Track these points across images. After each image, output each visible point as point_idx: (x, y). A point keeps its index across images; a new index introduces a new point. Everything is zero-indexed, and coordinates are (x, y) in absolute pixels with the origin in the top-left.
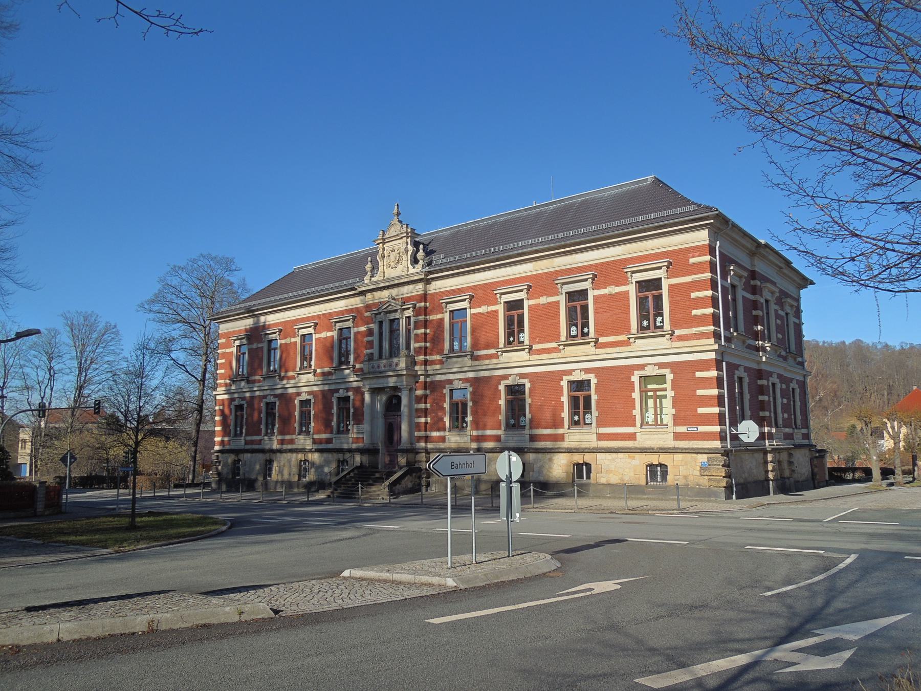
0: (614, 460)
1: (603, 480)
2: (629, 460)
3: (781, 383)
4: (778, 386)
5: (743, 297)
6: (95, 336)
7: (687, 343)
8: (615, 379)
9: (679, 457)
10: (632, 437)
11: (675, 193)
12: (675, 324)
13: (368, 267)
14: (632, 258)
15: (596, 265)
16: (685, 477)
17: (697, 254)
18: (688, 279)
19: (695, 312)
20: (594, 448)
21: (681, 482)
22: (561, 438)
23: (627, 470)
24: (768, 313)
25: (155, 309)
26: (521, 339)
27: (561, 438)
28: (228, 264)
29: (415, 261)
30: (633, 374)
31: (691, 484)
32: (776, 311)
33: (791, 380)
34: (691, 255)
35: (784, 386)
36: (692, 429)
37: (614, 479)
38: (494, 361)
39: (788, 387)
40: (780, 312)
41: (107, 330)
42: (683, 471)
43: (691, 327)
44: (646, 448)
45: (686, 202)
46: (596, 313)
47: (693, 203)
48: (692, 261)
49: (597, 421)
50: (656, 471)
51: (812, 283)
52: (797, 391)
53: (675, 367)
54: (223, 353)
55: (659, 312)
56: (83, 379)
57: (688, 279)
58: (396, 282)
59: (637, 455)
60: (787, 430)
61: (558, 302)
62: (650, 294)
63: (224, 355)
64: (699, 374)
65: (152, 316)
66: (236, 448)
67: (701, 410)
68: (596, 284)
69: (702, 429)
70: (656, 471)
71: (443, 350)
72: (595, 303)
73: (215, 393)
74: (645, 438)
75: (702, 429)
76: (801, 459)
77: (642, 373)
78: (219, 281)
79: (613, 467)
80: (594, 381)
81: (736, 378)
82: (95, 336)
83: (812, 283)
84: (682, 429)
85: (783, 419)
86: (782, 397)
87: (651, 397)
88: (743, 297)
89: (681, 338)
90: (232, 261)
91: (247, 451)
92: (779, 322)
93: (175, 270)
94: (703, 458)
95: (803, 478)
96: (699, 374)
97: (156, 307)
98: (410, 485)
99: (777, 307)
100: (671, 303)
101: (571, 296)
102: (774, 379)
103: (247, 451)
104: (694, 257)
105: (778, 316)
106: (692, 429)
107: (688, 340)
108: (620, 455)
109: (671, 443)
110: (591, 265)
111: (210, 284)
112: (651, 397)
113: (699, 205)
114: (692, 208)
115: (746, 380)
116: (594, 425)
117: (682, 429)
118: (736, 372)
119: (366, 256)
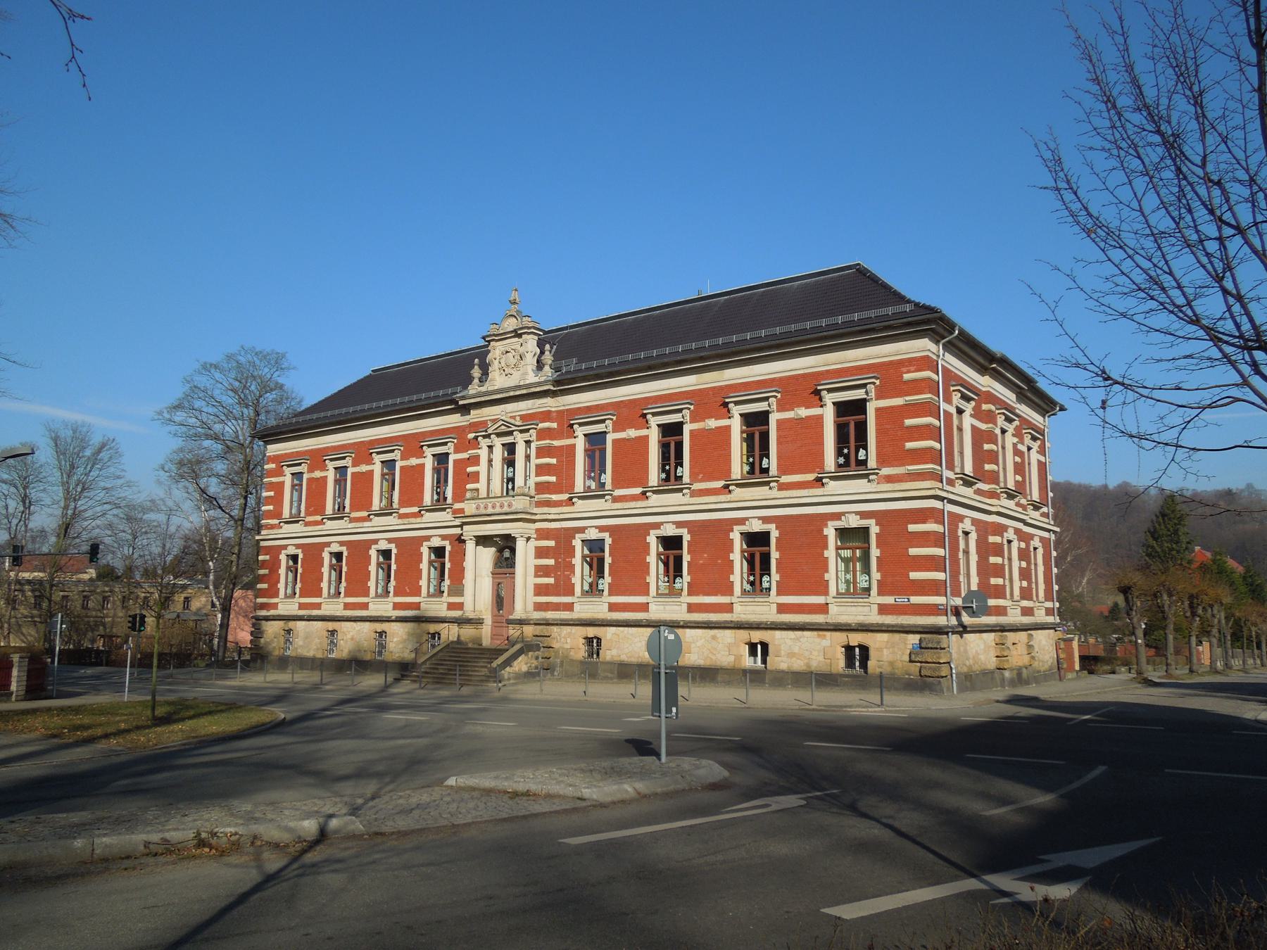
0: (798, 639)
1: (608, 658)
2: (818, 640)
3: (1020, 540)
4: (1015, 545)
5: (973, 426)
6: (88, 453)
7: (897, 486)
8: (804, 532)
9: (884, 637)
10: (570, 607)
11: (885, 286)
12: (883, 460)
13: (476, 372)
14: (827, 371)
15: (781, 379)
16: (891, 663)
17: (912, 368)
18: (898, 401)
19: (910, 445)
20: (772, 623)
21: (886, 669)
22: (275, 606)
23: (815, 653)
24: (1003, 448)
25: (177, 419)
26: (765, 465)
27: (275, 606)
28: (277, 361)
29: (540, 365)
30: (826, 526)
31: (898, 672)
32: (1015, 445)
33: (1032, 537)
34: (904, 370)
35: (1023, 545)
36: (902, 600)
37: (798, 665)
38: (275, 531)
39: (1028, 545)
40: (1020, 447)
41: (103, 446)
42: (887, 655)
43: (903, 465)
44: (840, 624)
45: (901, 299)
46: (779, 443)
47: (909, 301)
48: (907, 377)
49: (879, 587)
50: (857, 656)
51: (1062, 409)
52: (1040, 551)
53: (879, 516)
54: (271, 483)
55: (862, 442)
56: (70, 512)
57: (898, 401)
58: (512, 394)
59: (828, 634)
60: (1025, 603)
61: (647, 437)
62: (852, 420)
63: (272, 486)
64: (912, 528)
65: (173, 428)
66: (286, 613)
67: (914, 575)
68: (618, 427)
69: (916, 600)
70: (857, 656)
71: (729, 471)
72: (878, 417)
73: (257, 538)
74: (841, 612)
75: (916, 600)
76: (1044, 642)
77: (839, 524)
78: (265, 387)
79: (796, 650)
80: (775, 534)
81: (960, 533)
82: (88, 453)
83: (1062, 409)
84: (889, 600)
85: (1021, 588)
86: (1021, 559)
87: (854, 553)
88: (973, 426)
89: (890, 479)
90: (284, 356)
91: (301, 618)
92: (1018, 459)
93: (207, 368)
94: (914, 639)
95: (1046, 667)
96: (912, 528)
97: (180, 416)
98: (524, 668)
99: (1015, 440)
100: (878, 431)
101: (749, 419)
102: (1010, 534)
103: (301, 618)
104: (908, 372)
105: (1017, 452)
106: (902, 600)
107: (901, 481)
108: (806, 633)
109: (874, 618)
110: (773, 380)
111: (253, 388)
112: (854, 553)
113: (917, 305)
114: (908, 308)
115: (973, 537)
116: (606, 593)
117: (889, 600)
118: (961, 525)
119: (476, 356)
